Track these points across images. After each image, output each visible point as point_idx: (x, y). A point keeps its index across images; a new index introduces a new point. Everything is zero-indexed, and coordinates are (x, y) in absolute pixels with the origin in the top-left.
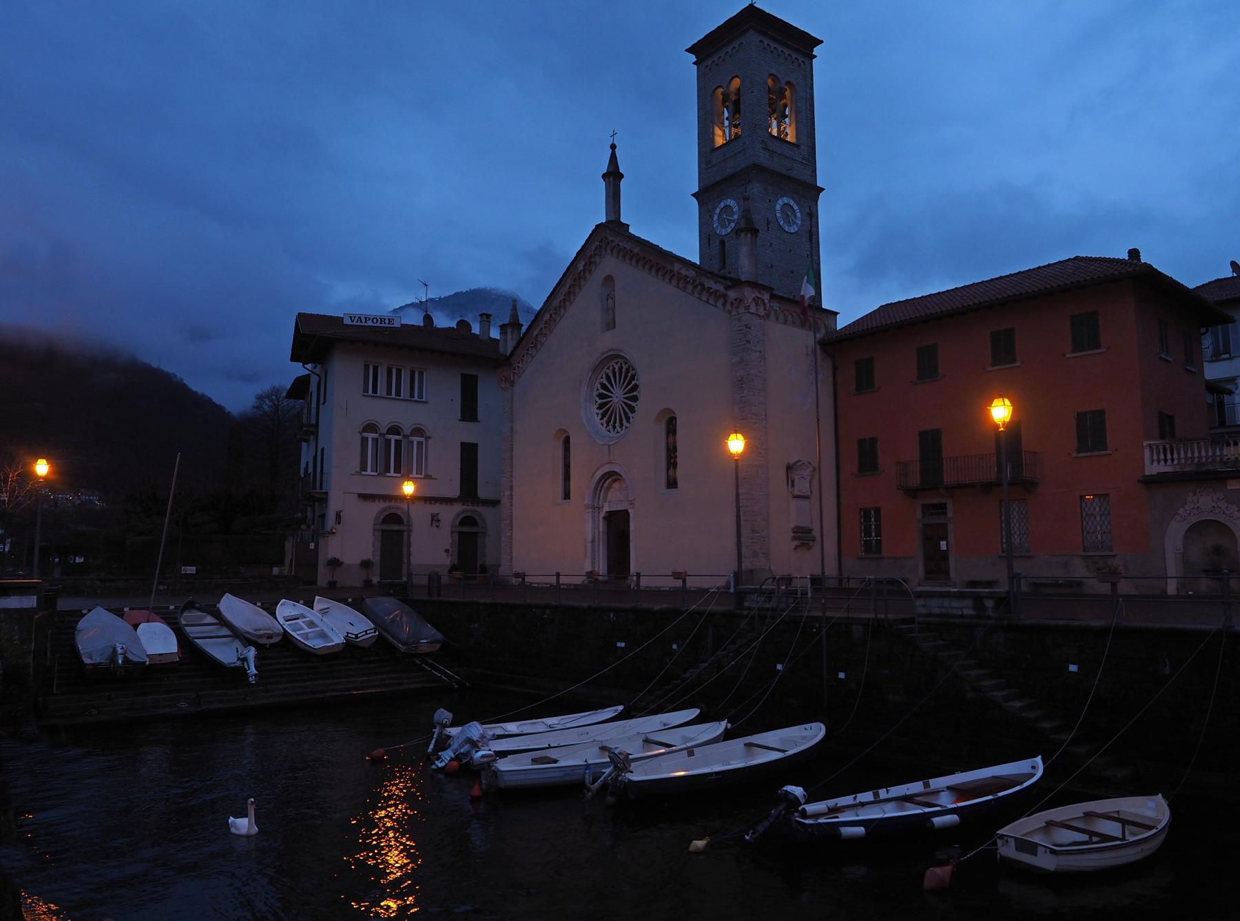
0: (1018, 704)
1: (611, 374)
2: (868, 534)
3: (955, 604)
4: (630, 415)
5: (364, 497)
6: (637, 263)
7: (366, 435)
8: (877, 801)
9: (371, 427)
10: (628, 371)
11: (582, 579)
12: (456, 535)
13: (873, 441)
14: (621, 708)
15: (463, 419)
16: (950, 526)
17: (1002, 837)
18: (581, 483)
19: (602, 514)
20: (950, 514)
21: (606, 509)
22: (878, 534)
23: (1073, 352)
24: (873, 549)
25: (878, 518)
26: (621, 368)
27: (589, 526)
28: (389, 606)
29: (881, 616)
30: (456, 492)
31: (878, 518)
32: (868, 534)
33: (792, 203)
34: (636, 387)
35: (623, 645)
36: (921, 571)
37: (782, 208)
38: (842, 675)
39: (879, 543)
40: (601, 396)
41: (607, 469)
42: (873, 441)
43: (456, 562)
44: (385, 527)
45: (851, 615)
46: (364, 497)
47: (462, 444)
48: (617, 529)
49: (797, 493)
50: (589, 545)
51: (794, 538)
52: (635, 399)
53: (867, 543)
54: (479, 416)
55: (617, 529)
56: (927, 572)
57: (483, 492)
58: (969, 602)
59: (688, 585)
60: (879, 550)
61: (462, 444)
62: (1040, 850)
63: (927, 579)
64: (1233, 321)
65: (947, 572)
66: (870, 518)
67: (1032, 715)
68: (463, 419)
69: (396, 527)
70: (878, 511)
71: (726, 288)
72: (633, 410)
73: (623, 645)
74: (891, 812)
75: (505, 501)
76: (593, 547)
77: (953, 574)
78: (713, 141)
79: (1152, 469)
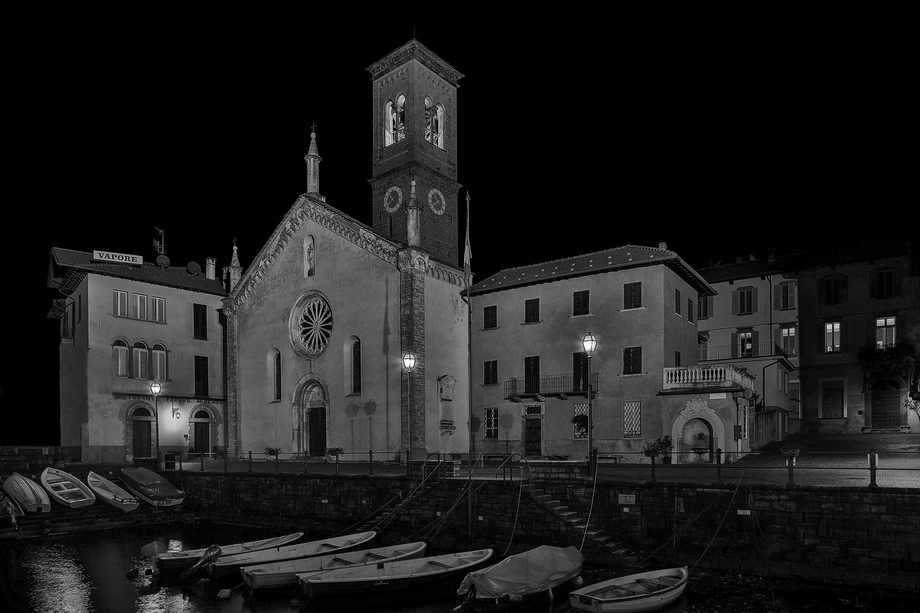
1: (312, 309)
3: (554, 470)
5: (118, 395)
11: (291, 456)
13: (495, 363)
16: (543, 421)
18: (290, 388)
19: (305, 411)
20: (543, 413)
22: (496, 425)
23: (625, 308)
25: (496, 415)
26: (319, 305)
27: (295, 419)
29: (508, 479)
31: (496, 415)
33: (440, 193)
35: (326, 501)
37: (433, 196)
38: (481, 518)
39: (496, 431)
41: (309, 377)
42: (495, 363)
46: (118, 395)
48: (317, 420)
49: (444, 397)
50: (296, 432)
51: (442, 428)
52: (330, 328)
53: (489, 432)
55: (317, 420)
56: (527, 450)
57: (215, 389)
60: (496, 436)
64: (713, 293)
67: (602, 539)
69: (144, 418)
70: (496, 411)
73: (326, 501)
76: (299, 433)
77: (543, 452)
79: (667, 386)
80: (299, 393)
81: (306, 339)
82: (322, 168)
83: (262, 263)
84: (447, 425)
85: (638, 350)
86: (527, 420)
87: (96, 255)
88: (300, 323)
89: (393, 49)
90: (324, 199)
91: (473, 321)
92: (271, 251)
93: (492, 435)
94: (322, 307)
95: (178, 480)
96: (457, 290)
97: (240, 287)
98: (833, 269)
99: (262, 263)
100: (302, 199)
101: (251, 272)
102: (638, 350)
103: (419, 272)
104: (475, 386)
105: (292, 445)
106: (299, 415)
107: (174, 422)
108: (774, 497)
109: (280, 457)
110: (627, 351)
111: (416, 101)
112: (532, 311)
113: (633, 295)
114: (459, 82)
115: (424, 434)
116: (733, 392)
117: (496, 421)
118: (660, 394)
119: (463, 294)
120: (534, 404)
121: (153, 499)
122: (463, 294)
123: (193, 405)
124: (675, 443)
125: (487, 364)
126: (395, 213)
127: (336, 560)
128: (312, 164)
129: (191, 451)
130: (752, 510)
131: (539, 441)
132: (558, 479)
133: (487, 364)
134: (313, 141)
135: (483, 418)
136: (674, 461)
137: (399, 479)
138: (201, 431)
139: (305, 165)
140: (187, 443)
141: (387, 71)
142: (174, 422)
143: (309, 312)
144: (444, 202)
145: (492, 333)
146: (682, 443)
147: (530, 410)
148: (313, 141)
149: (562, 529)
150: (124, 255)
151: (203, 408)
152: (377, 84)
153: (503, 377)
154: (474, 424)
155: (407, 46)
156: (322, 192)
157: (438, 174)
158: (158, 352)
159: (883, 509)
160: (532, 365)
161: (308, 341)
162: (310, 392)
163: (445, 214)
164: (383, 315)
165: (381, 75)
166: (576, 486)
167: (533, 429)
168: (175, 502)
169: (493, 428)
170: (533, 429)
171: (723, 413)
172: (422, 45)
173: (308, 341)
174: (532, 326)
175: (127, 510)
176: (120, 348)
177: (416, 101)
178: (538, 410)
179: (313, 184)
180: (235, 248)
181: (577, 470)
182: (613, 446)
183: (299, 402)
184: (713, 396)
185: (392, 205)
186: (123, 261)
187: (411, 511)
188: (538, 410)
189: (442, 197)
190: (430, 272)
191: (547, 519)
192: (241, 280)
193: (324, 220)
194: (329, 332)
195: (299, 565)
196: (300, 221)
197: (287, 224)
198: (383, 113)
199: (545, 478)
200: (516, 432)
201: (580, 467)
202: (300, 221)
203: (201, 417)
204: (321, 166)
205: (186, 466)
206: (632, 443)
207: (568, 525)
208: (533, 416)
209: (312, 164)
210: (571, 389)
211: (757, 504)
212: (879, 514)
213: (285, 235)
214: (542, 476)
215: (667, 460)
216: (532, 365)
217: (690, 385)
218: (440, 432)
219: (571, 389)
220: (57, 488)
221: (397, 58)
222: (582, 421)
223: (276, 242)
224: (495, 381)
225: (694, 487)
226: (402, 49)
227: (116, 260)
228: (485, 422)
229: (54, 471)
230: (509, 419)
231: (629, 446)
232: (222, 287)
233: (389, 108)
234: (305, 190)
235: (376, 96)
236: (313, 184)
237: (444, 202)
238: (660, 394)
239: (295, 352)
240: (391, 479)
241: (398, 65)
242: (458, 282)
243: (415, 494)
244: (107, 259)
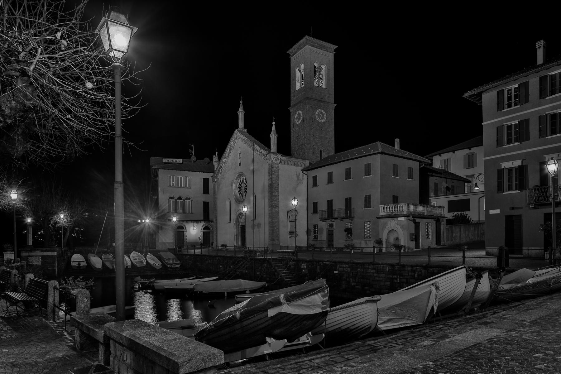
53: (315, 236)
57: (211, 217)
79: (381, 214)
82: (245, 116)
84: (293, 233)
85: (370, 196)
86: (329, 230)
87: (164, 160)
89: (297, 42)
90: (246, 130)
92: (227, 155)
93: (316, 237)
96: (299, 169)
98: (470, 149)
102: (370, 196)
103: (276, 164)
104: (309, 214)
107: (194, 231)
108: (344, 266)
109: (227, 248)
110: (366, 197)
111: (312, 65)
112: (348, 174)
113: (368, 170)
114: (335, 50)
115: (279, 238)
116: (407, 217)
118: (378, 218)
119: (303, 170)
120: (331, 223)
122: (303, 170)
123: (202, 224)
124: (384, 243)
125: (314, 203)
126: (299, 124)
128: (241, 114)
129: (201, 244)
130: (338, 271)
131: (333, 241)
133: (314, 203)
134: (241, 105)
135: (311, 228)
136: (384, 251)
138: (206, 235)
140: (200, 241)
141: (296, 52)
142: (194, 231)
144: (325, 115)
145: (315, 188)
146: (387, 241)
148: (241, 105)
151: (207, 225)
152: (292, 59)
153: (319, 209)
154: (308, 232)
155: (304, 39)
156: (245, 127)
157: (321, 101)
158: (188, 201)
159: (374, 271)
160: (330, 203)
163: (326, 121)
164: (386, 152)
165: (294, 55)
167: (330, 234)
168: (177, 266)
170: (330, 234)
171: (402, 227)
172: (311, 38)
174: (330, 185)
175: (158, 268)
176: (172, 200)
177: (312, 65)
179: (241, 124)
180: (274, 123)
182: (360, 243)
184: (399, 219)
185: (298, 120)
189: (324, 113)
190: (283, 162)
193: (243, 140)
197: (231, 143)
198: (295, 74)
200: (324, 236)
204: (245, 116)
206: (368, 242)
208: (331, 229)
209: (241, 114)
210: (344, 216)
211: (340, 269)
212: (374, 273)
213: (232, 147)
215: (381, 250)
216: (330, 203)
217: (390, 214)
218: (289, 236)
219: (344, 216)
220: (136, 259)
221: (300, 45)
222: (349, 231)
225: (322, 261)
226: (302, 41)
227: (171, 162)
228: (312, 231)
229: (136, 252)
230: (322, 229)
231: (366, 243)
232: (211, 169)
233: (297, 72)
234: (237, 127)
235: (292, 65)
236: (241, 124)
237: (325, 115)
238: (378, 218)
241: (301, 49)
242: (300, 165)
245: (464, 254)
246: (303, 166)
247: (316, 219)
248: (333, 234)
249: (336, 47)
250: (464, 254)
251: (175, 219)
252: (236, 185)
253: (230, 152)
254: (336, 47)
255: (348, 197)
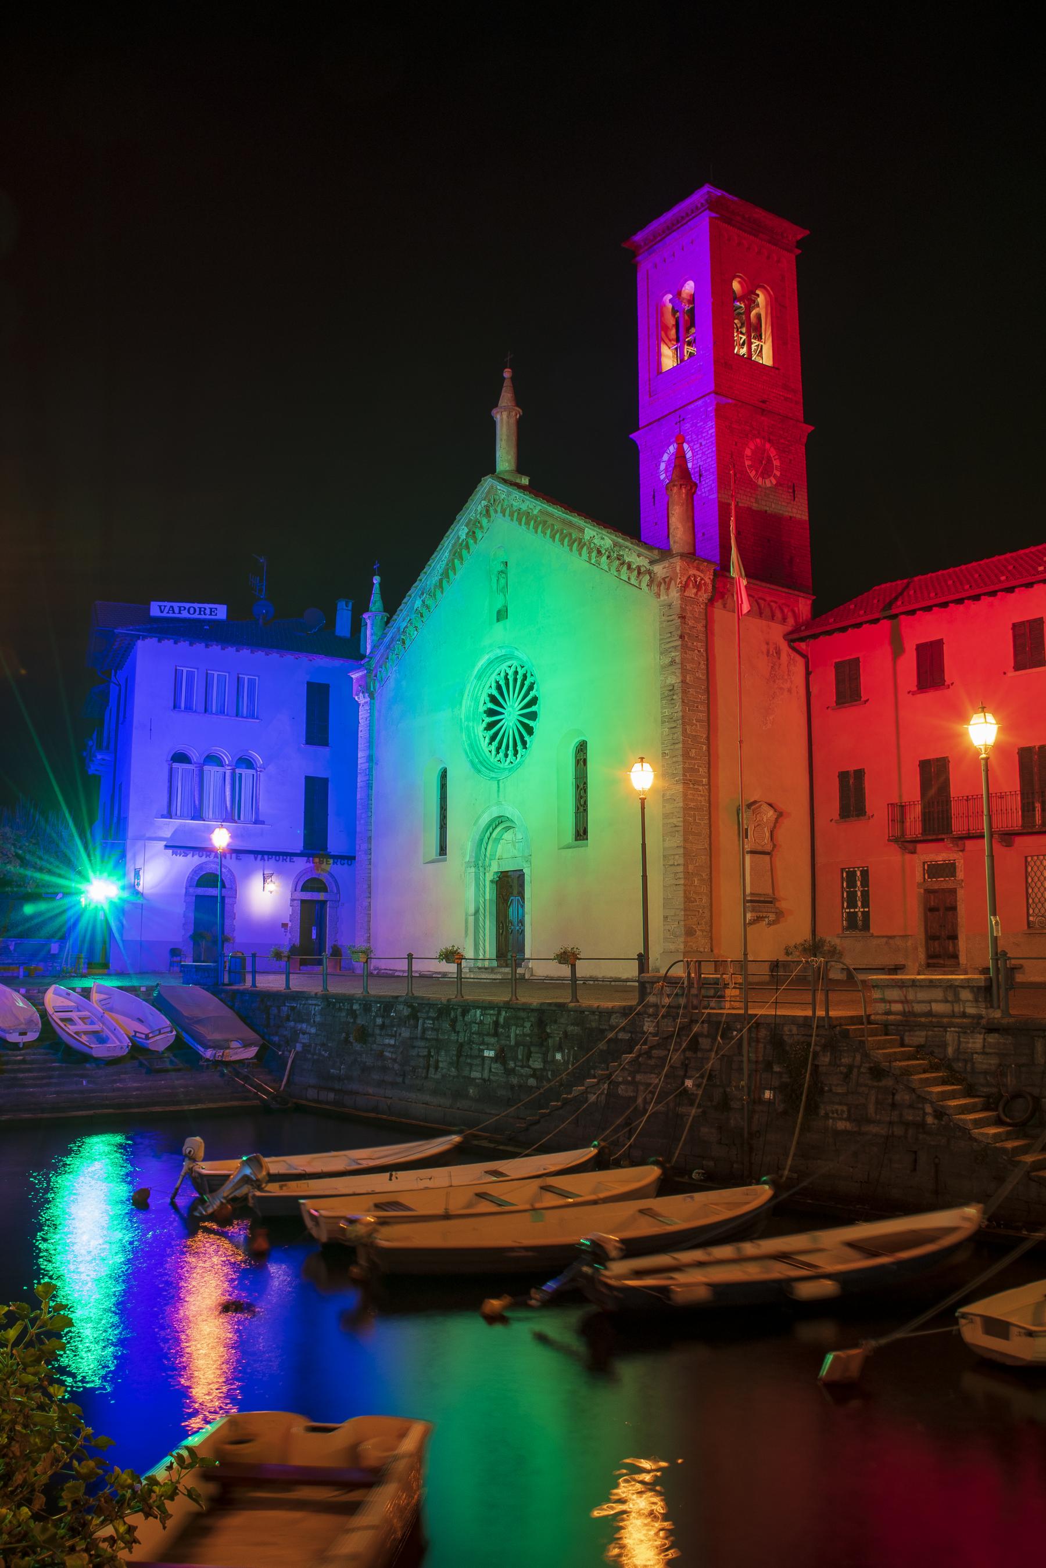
0: (992, 1131)
2: (852, 904)
3: (922, 995)
4: (527, 738)
6: (536, 528)
7: (175, 765)
8: (741, 1260)
9: (181, 757)
10: (525, 677)
12: (297, 903)
13: (859, 774)
14: (456, 1139)
15: (310, 741)
16: (961, 893)
17: (964, 1316)
19: (490, 876)
20: (960, 875)
21: (495, 868)
22: (866, 903)
24: (857, 924)
28: (201, 1003)
30: (299, 846)
32: (852, 904)
34: (534, 701)
35: (492, 1054)
36: (922, 956)
39: (866, 916)
40: (491, 713)
41: (495, 812)
42: (859, 774)
43: (297, 943)
44: (201, 891)
45: (780, 1012)
47: (307, 777)
50: (471, 919)
52: (533, 716)
53: (852, 918)
54: (836, 782)
56: (930, 956)
57: (335, 843)
58: (938, 994)
59: (579, 974)
60: (866, 927)
61: (307, 777)
62: (1014, 1331)
63: (928, 965)
65: (955, 956)
66: (856, 884)
68: (310, 741)
70: (865, 874)
71: (652, 562)
72: (530, 731)
74: (752, 1272)
75: (360, 856)
76: (476, 921)
77: (963, 959)
78: (659, 364)
80: (481, 844)
81: (493, 738)
83: (418, 603)
88: (482, 708)
91: (814, 690)
92: (435, 580)
94: (520, 677)
95: (256, 1011)
97: (382, 648)
99: (418, 603)
100: (488, 482)
101: (401, 619)
104: (819, 823)
105: (479, 947)
106: (477, 885)
114: (799, 244)
117: (865, 895)
121: (206, 1047)
125: (843, 776)
127: (546, 1188)
128: (504, 422)
131: (954, 937)
132: (929, 1014)
133: (843, 776)
134: (507, 384)
137: (625, 1012)
139: (493, 424)
143: (499, 688)
147: (935, 870)
148: (507, 384)
149: (930, 1120)
150: (196, 606)
153: (876, 803)
156: (521, 468)
161: (495, 743)
162: (498, 840)
166: (964, 1030)
169: (859, 910)
173: (495, 743)
178: (950, 869)
179: (505, 458)
180: (377, 580)
181: (966, 995)
183: (479, 863)
186: (196, 616)
187: (638, 1077)
188: (950, 869)
189: (773, 453)
191: (898, 1097)
192: (384, 635)
194: (531, 723)
195: (406, 1180)
196: (484, 521)
197: (460, 530)
199: (903, 1013)
201: (971, 988)
202: (484, 521)
203: (313, 890)
205: (271, 982)
207: (939, 1114)
208: (942, 883)
209: (504, 422)
214: (897, 1007)
223: (443, 564)
224: (860, 811)
234: (490, 468)
236: (505, 458)
239: (472, 762)
240: (610, 1013)
243: (645, 1043)
244: (171, 615)
245: (410, 965)
246: (791, 621)
247: (867, 843)
248: (953, 908)
249: (802, 234)
250: (410, 965)
251: (982, 731)
252: (476, 700)
253: (450, 567)
254: (802, 234)
255: (852, 768)
